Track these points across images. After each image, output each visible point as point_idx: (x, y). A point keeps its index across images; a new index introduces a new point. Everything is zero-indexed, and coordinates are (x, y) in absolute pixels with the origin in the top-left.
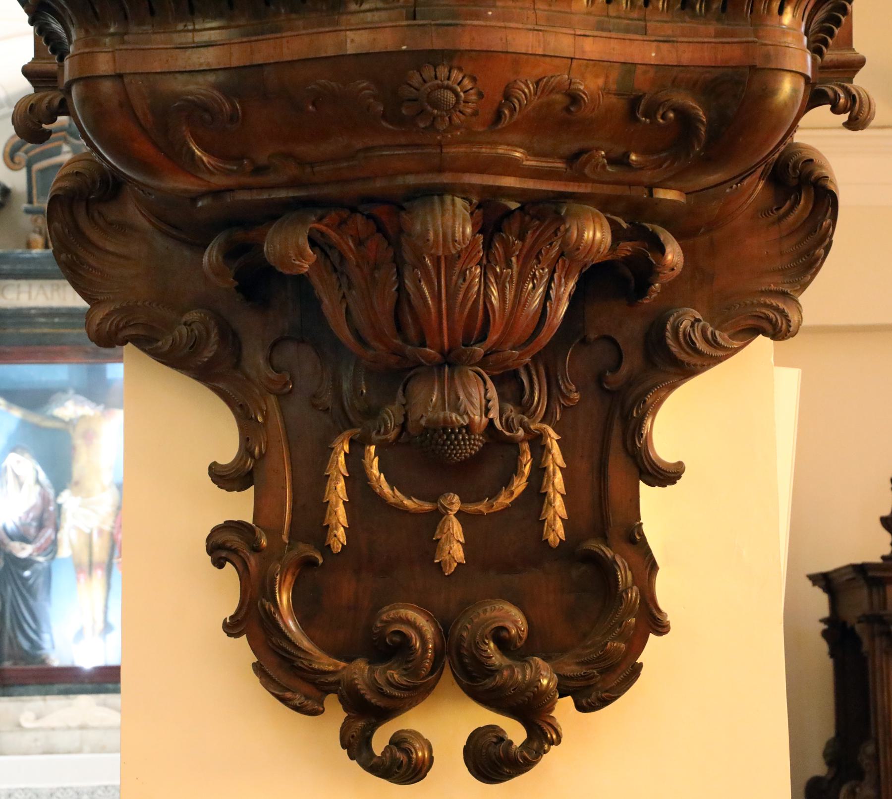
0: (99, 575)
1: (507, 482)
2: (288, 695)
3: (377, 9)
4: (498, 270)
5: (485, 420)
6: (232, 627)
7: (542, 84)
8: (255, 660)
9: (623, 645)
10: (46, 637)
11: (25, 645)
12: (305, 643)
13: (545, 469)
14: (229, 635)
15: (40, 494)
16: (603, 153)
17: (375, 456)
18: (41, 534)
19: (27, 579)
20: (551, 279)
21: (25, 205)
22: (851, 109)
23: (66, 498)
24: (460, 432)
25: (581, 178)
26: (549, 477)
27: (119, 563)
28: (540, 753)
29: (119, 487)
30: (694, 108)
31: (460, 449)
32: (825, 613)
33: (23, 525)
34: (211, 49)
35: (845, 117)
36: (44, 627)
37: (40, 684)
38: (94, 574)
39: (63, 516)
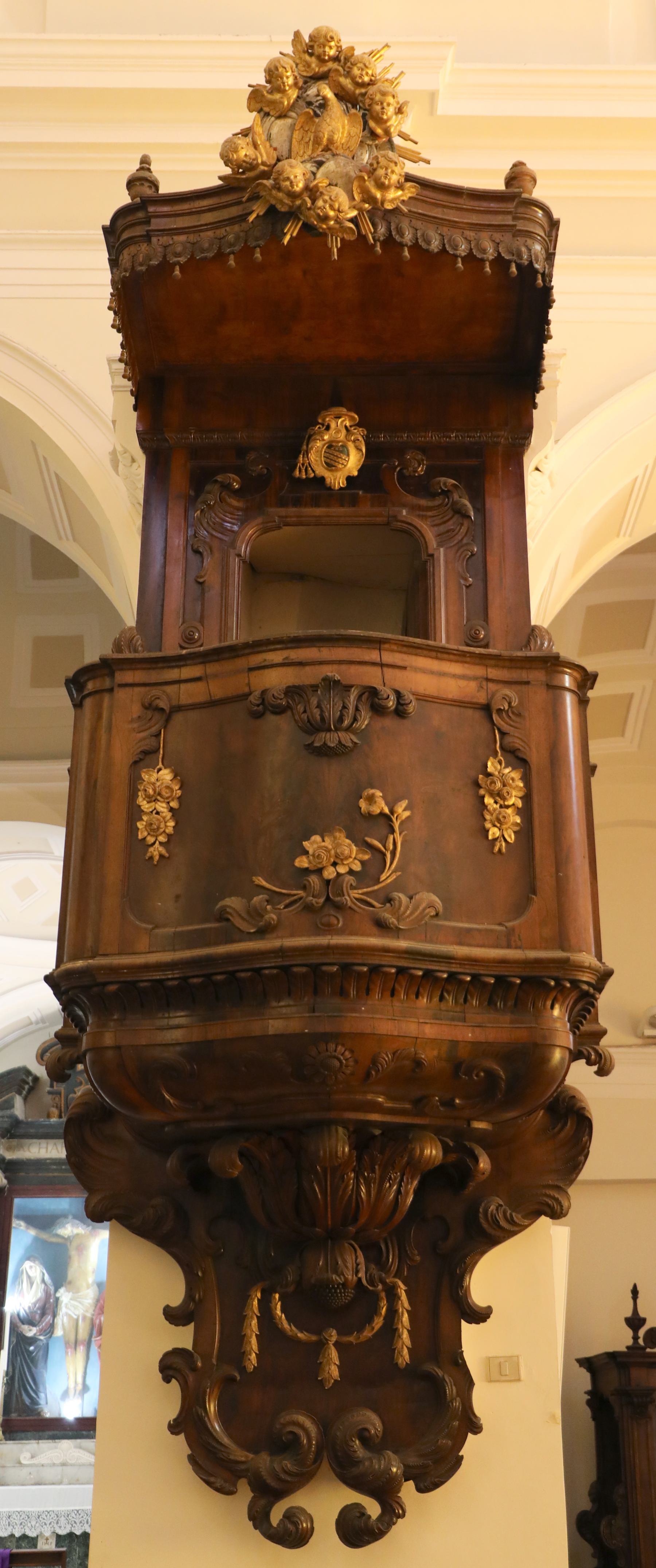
0: (81, 1349)
1: (370, 1320)
2: (212, 1479)
3: (289, 1006)
4: (366, 1174)
5: (355, 1278)
6: (175, 1428)
7: (397, 1054)
8: (190, 1452)
9: (450, 1442)
10: (42, 1395)
11: (27, 1401)
12: (226, 1440)
13: (396, 1311)
14: (172, 1433)
15: (44, 1290)
16: (437, 1098)
17: (279, 1300)
18: (43, 1319)
19: (32, 1352)
20: (402, 1180)
21: (48, 1089)
22: (599, 1062)
23: (64, 1295)
24: (338, 1287)
25: (421, 1114)
26: (399, 1316)
27: (96, 1340)
28: (390, 1524)
29: (100, 1285)
30: (497, 1070)
31: (338, 1299)
32: (589, 1387)
33: (31, 1313)
34: (179, 1030)
35: (595, 1068)
36: (41, 1388)
37: (36, 1431)
39: (59, 1306)
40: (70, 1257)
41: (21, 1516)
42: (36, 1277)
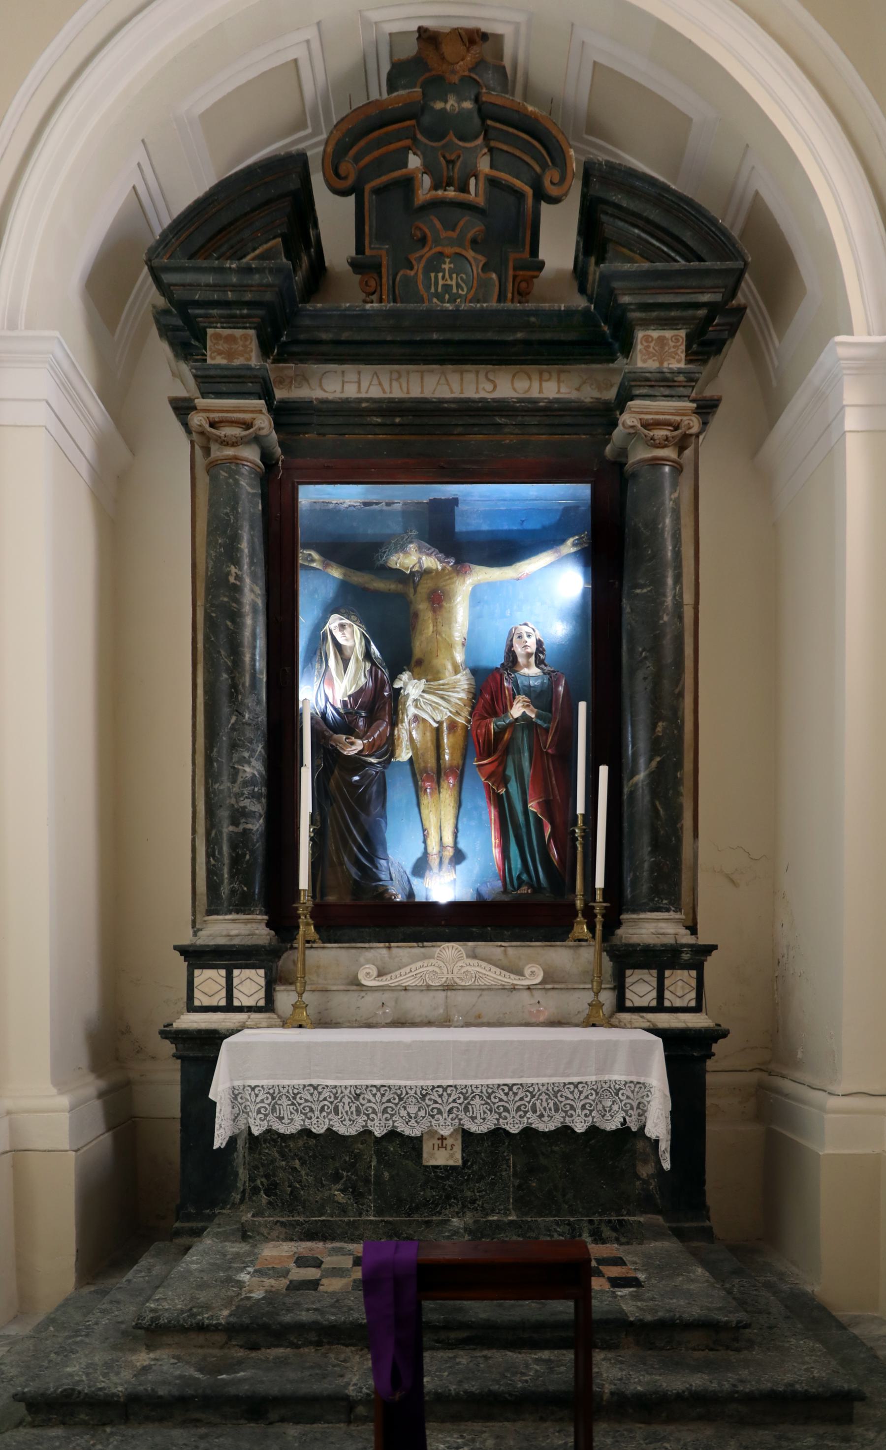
38: (444, 784)
40: (416, 615)
41: (383, 1095)
42: (353, 648)
